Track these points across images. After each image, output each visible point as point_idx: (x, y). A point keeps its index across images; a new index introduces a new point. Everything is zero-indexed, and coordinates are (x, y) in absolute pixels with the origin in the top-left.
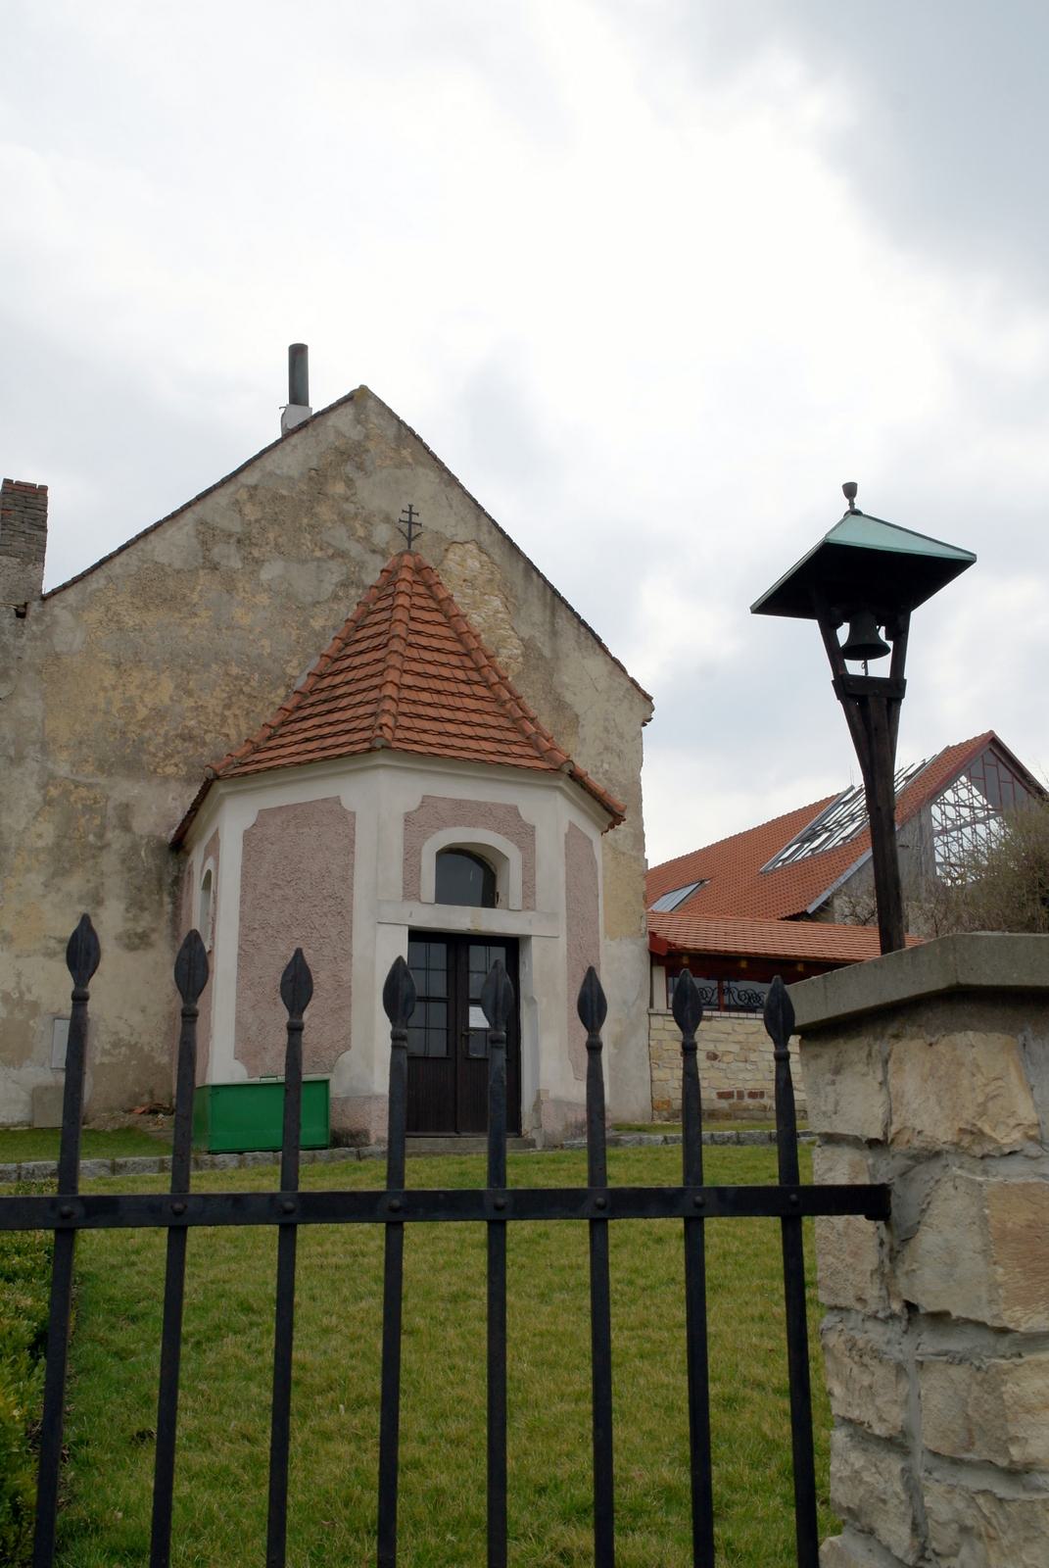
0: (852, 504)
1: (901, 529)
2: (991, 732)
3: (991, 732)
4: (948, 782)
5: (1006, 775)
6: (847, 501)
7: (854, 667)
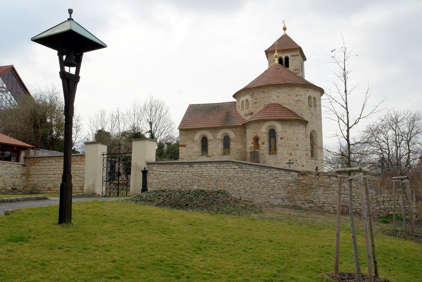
0: (70, 16)
2: (12, 65)
5: (15, 80)
6: (69, 15)
7: (67, 69)
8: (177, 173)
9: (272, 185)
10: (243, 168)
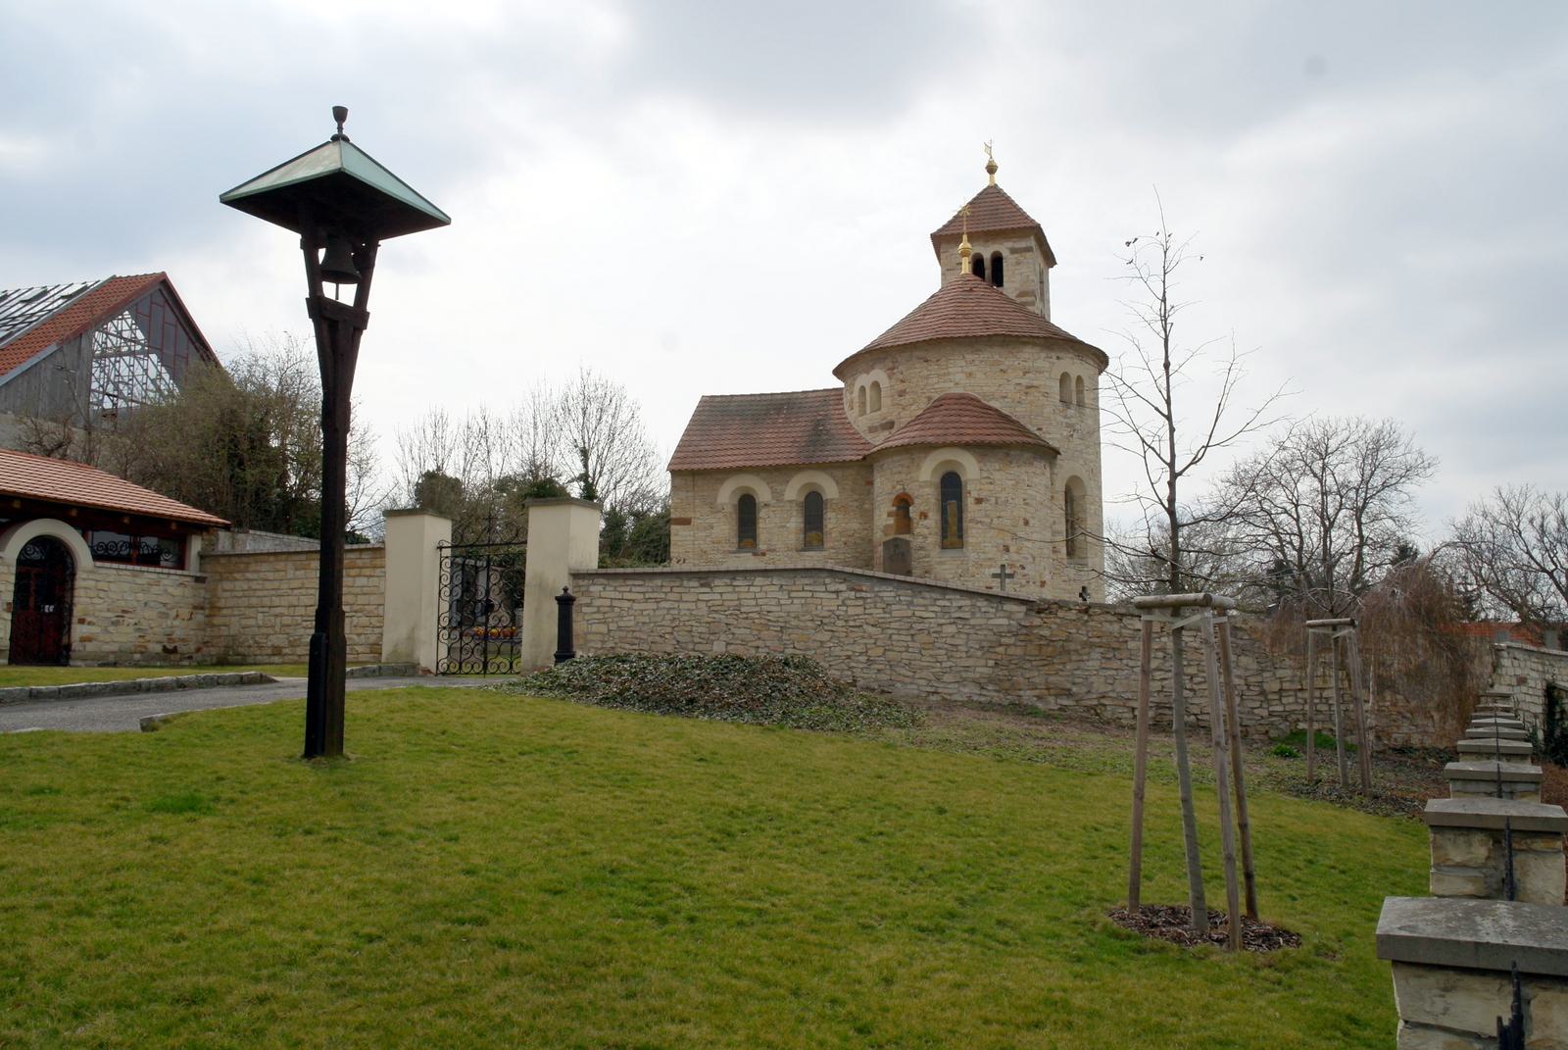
0: (340, 128)
1: (358, 149)
2: (163, 274)
3: (163, 274)
4: (113, 313)
5: (170, 317)
6: (336, 124)
7: (329, 289)
8: (663, 604)
9: (949, 641)
10: (862, 591)
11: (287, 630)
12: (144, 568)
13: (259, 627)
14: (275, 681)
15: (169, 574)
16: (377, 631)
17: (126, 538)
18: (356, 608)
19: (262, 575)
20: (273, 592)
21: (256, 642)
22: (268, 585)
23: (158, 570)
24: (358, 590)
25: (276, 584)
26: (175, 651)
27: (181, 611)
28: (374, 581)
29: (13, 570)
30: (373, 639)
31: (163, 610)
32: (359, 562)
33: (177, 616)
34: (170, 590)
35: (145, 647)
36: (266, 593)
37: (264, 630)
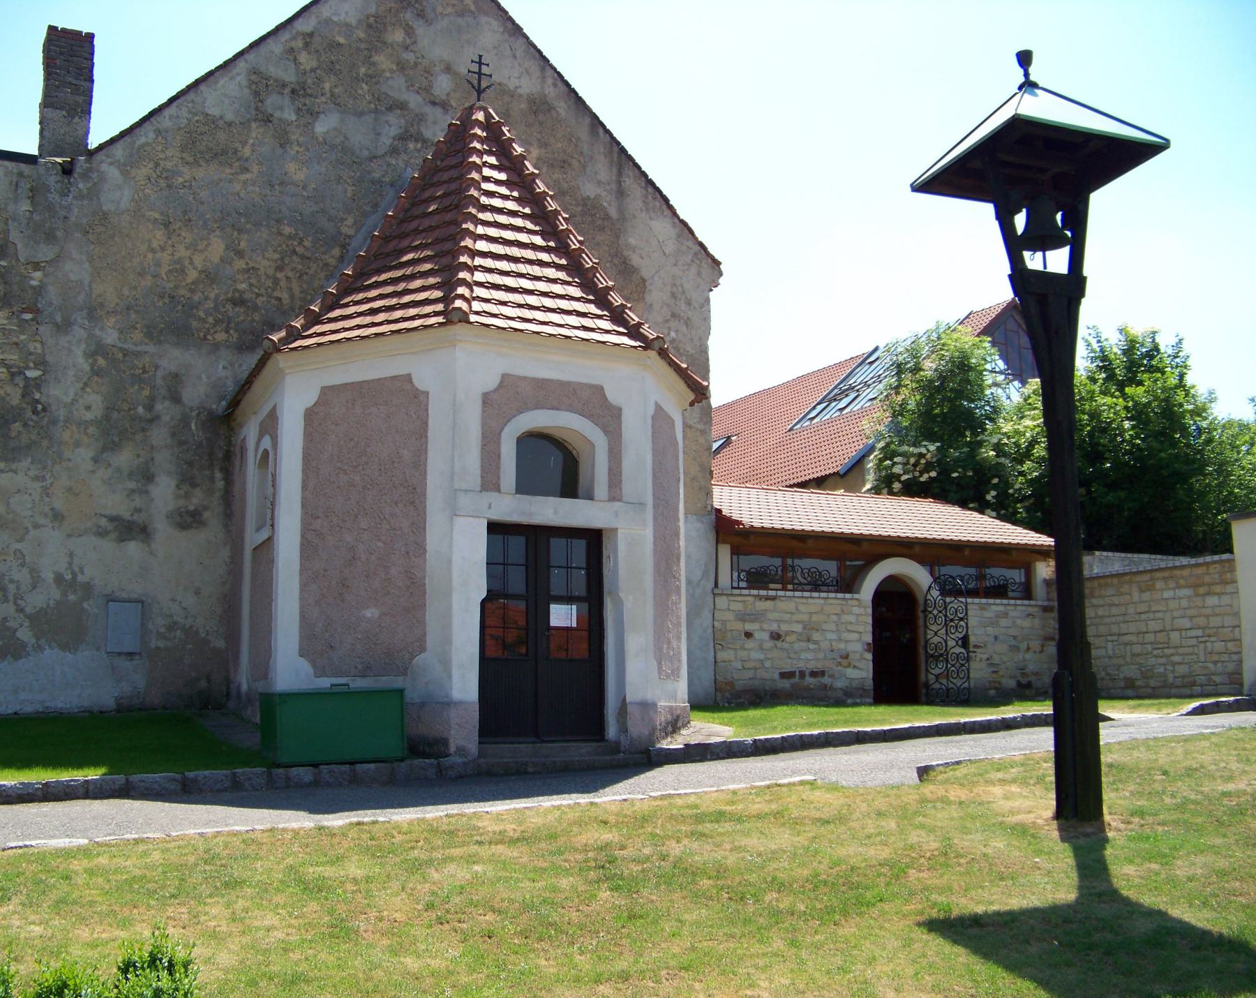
0: (1026, 75)
6: (1021, 71)
7: (1033, 261)
11: (1138, 660)
12: (991, 601)
13: (1110, 657)
14: (1110, 719)
15: (1016, 605)
16: (1235, 657)
17: (972, 571)
18: (1208, 632)
19: (1107, 600)
20: (1121, 618)
21: (1108, 674)
22: (1114, 611)
23: (1005, 601)
24: (1208, 611)
25: (1122, 610)
26: (1029, 685)
27: (1032, 644)
28: (1226, 600)
29: (870, 611)
30: (1231, 667)
31: (1014, 643)
32: (1207, 579)
33: (1028, 649)
34: (1019, 622)
35: (1000, 683)
36: (1113, 619)
37: (1115, 661)
